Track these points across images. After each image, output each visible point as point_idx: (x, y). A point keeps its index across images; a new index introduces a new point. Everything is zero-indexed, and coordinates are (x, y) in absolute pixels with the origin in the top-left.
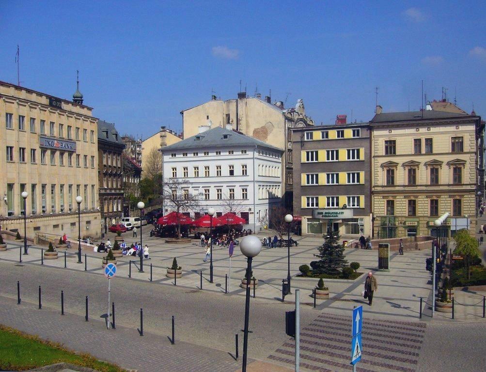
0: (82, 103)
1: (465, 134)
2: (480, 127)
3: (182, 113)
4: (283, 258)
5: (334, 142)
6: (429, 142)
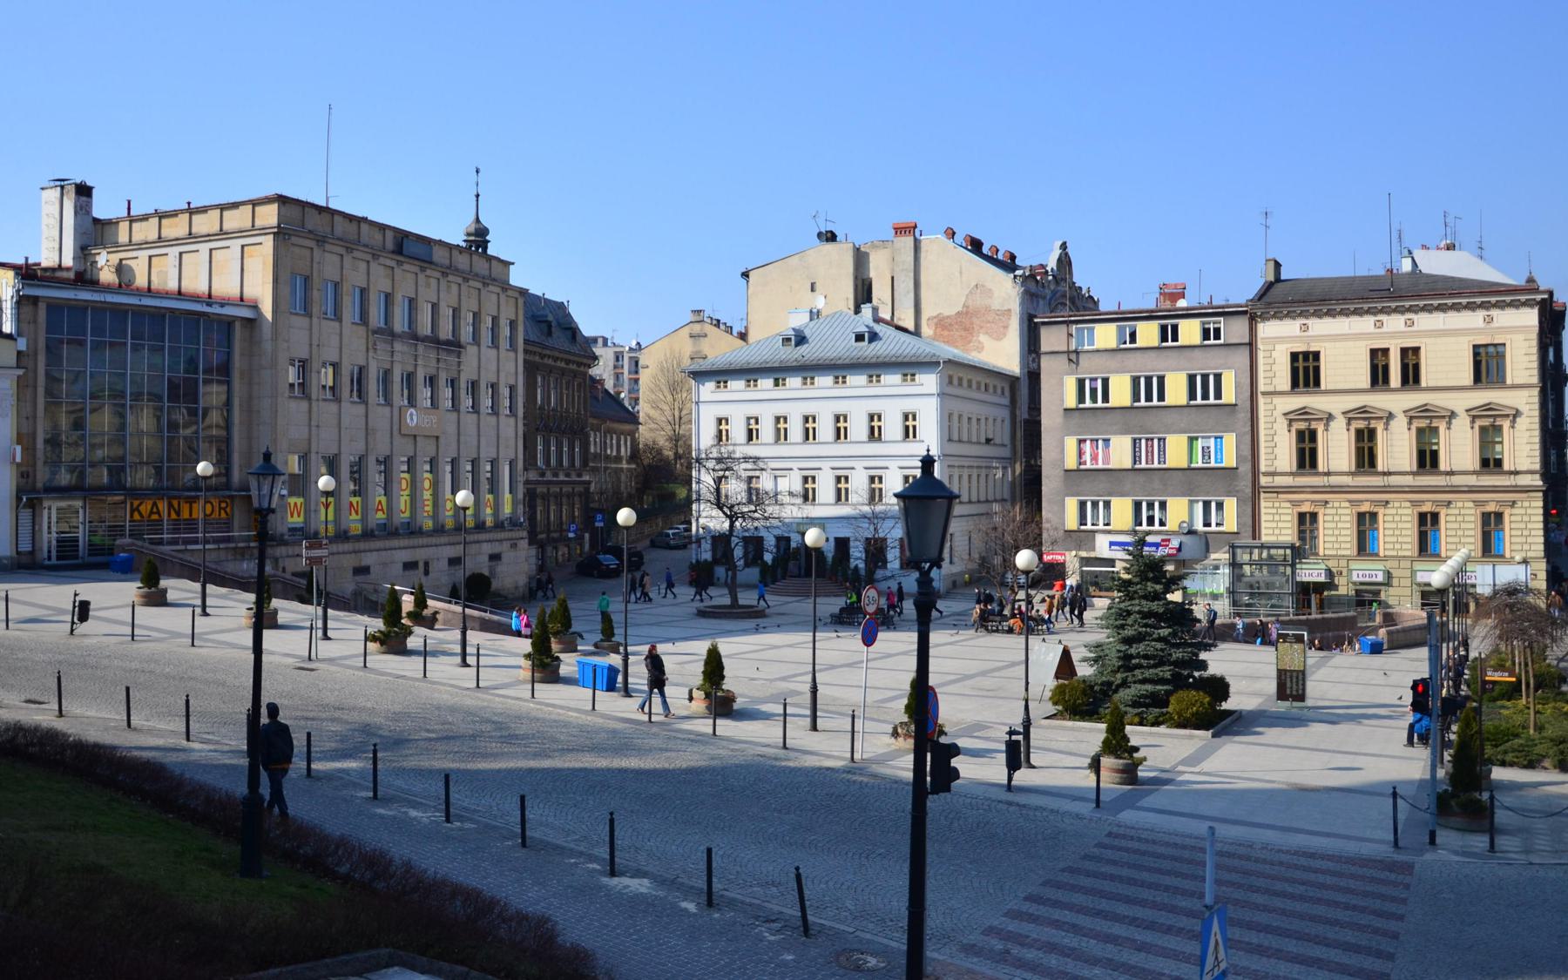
0: (485, 248)
1: (1514, 337)
2: (1551, 321)
3: (746, 275)
4: (1013, 664)
5: (1153, 354)
6: (1410, 359)
